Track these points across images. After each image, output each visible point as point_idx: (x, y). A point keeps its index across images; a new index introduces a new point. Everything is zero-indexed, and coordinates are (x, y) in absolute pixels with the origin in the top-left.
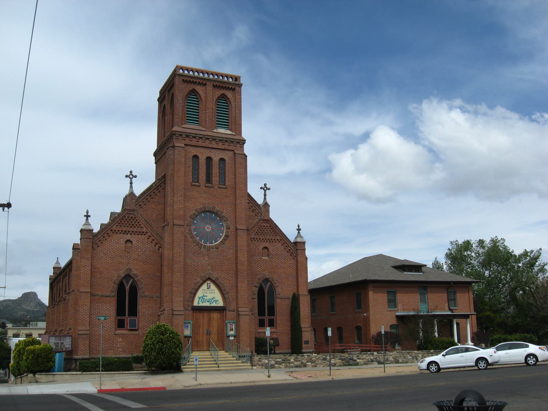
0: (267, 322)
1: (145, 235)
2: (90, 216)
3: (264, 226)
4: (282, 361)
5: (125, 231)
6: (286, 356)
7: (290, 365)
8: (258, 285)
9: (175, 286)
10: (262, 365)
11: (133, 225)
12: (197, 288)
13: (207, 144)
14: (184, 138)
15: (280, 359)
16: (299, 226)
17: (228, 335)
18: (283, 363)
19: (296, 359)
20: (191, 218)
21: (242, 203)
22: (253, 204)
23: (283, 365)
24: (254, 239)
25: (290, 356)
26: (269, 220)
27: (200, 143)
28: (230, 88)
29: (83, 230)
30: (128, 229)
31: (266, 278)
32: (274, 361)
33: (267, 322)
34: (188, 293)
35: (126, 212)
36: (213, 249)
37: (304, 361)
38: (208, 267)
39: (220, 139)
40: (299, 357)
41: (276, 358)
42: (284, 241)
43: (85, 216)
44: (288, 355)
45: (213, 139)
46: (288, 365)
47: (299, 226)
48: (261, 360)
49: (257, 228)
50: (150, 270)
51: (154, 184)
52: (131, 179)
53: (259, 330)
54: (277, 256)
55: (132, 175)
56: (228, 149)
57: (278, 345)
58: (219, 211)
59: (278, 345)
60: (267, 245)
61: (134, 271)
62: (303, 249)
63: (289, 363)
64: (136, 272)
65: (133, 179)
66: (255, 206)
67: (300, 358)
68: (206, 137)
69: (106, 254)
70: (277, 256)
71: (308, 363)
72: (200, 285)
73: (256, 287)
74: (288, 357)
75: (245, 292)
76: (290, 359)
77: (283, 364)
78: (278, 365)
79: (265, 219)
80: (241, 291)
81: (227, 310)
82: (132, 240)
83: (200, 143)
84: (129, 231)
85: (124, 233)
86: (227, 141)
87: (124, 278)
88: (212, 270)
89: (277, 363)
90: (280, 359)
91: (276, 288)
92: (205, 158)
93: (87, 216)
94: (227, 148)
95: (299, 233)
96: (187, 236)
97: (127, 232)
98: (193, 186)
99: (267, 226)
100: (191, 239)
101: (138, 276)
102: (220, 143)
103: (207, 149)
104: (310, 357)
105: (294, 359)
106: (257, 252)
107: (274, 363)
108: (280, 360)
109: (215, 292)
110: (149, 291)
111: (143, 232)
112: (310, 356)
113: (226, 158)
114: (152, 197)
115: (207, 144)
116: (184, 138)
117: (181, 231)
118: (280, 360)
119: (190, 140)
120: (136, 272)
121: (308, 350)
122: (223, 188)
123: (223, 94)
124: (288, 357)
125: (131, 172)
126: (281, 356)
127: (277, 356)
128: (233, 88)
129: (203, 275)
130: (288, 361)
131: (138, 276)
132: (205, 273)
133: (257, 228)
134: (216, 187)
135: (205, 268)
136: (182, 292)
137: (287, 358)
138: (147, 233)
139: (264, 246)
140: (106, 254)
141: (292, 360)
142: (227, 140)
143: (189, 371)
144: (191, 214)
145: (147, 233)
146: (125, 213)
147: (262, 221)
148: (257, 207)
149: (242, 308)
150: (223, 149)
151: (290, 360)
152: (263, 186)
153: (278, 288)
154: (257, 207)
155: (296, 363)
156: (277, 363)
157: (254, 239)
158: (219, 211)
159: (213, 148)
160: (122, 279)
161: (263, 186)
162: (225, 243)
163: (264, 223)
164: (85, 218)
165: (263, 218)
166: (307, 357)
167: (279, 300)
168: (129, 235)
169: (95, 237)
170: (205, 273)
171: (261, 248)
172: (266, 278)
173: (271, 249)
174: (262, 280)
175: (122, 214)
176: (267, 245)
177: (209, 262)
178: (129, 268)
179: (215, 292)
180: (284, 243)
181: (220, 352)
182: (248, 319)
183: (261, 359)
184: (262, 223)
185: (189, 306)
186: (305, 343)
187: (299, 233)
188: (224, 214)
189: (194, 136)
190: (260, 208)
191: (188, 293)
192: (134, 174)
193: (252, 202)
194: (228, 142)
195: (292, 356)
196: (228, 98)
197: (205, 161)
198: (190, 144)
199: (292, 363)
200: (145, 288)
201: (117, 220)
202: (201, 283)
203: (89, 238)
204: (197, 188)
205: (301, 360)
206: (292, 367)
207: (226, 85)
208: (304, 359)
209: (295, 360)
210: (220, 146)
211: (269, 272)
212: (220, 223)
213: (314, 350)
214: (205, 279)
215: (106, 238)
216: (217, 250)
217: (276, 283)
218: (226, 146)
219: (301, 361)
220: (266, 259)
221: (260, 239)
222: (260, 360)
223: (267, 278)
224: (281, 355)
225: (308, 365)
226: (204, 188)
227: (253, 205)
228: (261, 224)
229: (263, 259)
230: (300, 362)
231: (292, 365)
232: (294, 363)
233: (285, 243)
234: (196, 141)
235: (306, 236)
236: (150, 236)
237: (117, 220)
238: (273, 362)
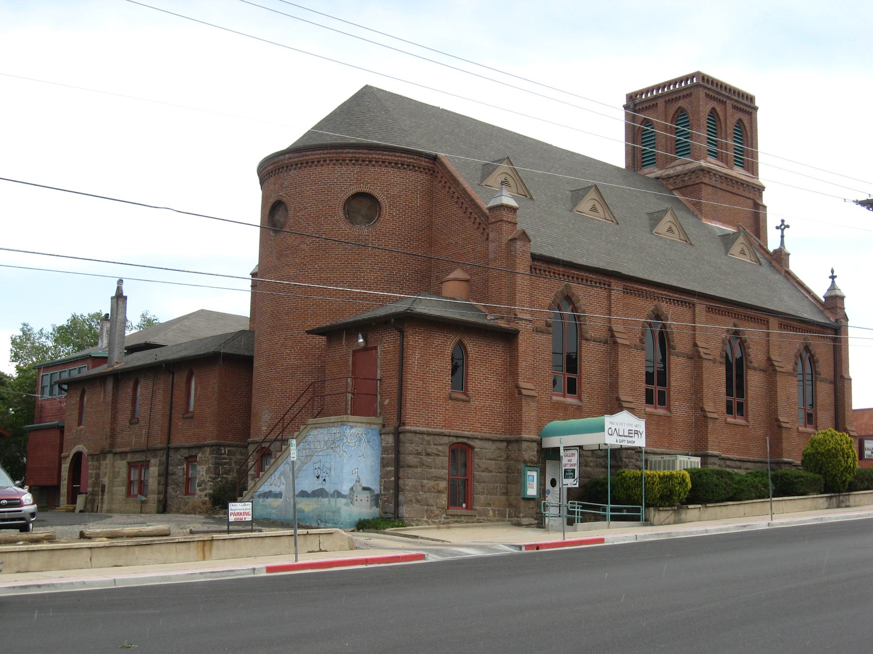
0: (656, 396)
2: (836, 277)
16: (832, 271)
27: (740, 192)
29: (503, 206)
33: (656, 396)
43: (830, 277)
47: (832, 271)
52: (783, 230)
55: (784, 228)
62: (833, 308)
65: (785, 231)
85: (341, 164)
93: (833, 277)
95: (833, 282)
109: (634, 430)
110: (491, 384)
125: (788, 226)
152: (786, 223)
161: (786, 223)
164: (831, 280)
179: (634, 430)
187: (833, 282)
192: (779, 224)
235: (843, 287)
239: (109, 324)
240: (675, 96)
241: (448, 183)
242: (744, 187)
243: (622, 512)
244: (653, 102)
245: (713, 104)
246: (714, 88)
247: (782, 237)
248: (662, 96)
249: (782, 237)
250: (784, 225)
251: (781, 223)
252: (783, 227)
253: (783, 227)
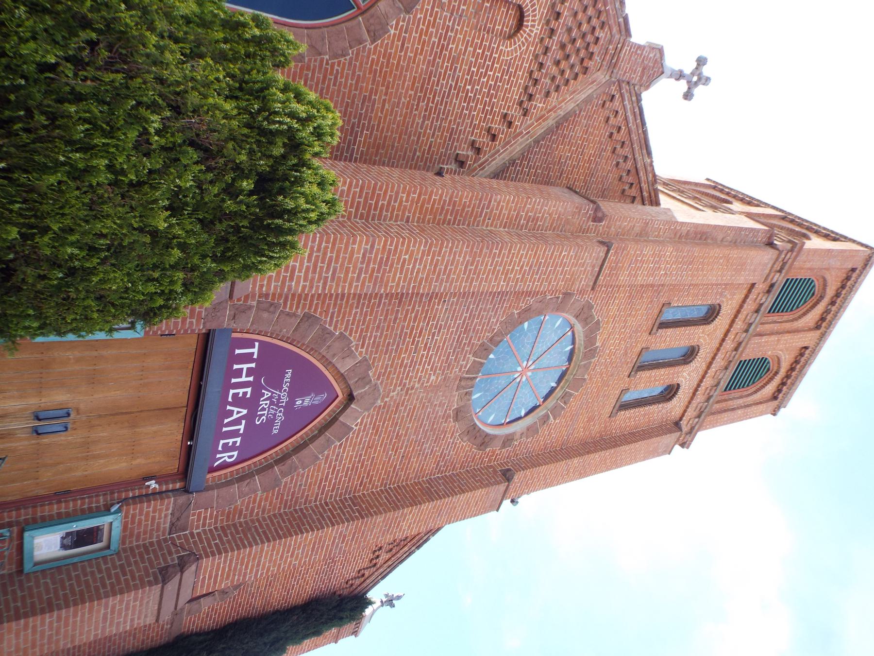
1: (521, 103)
9: (372, 246)
11: (567, 57)
30: (561, 35)
50: (387, 106)
51: (649, 161)
53: (56, 518)
55: (696, 84)
61: (397, 24)
64: (392, 32)
81: (182, 499)
82: (522, 36)
101: (373, 41)
111: (531, 97)
114: (483, 140)
120: (392, 32)
131: (373, 41)
136: (338, 285)
138: (525, 113)
145: (525, 113)
175: (616, 16)
200: (308, 69)
213: (80, 34)
216: (449, 416)
236: (510, 124)
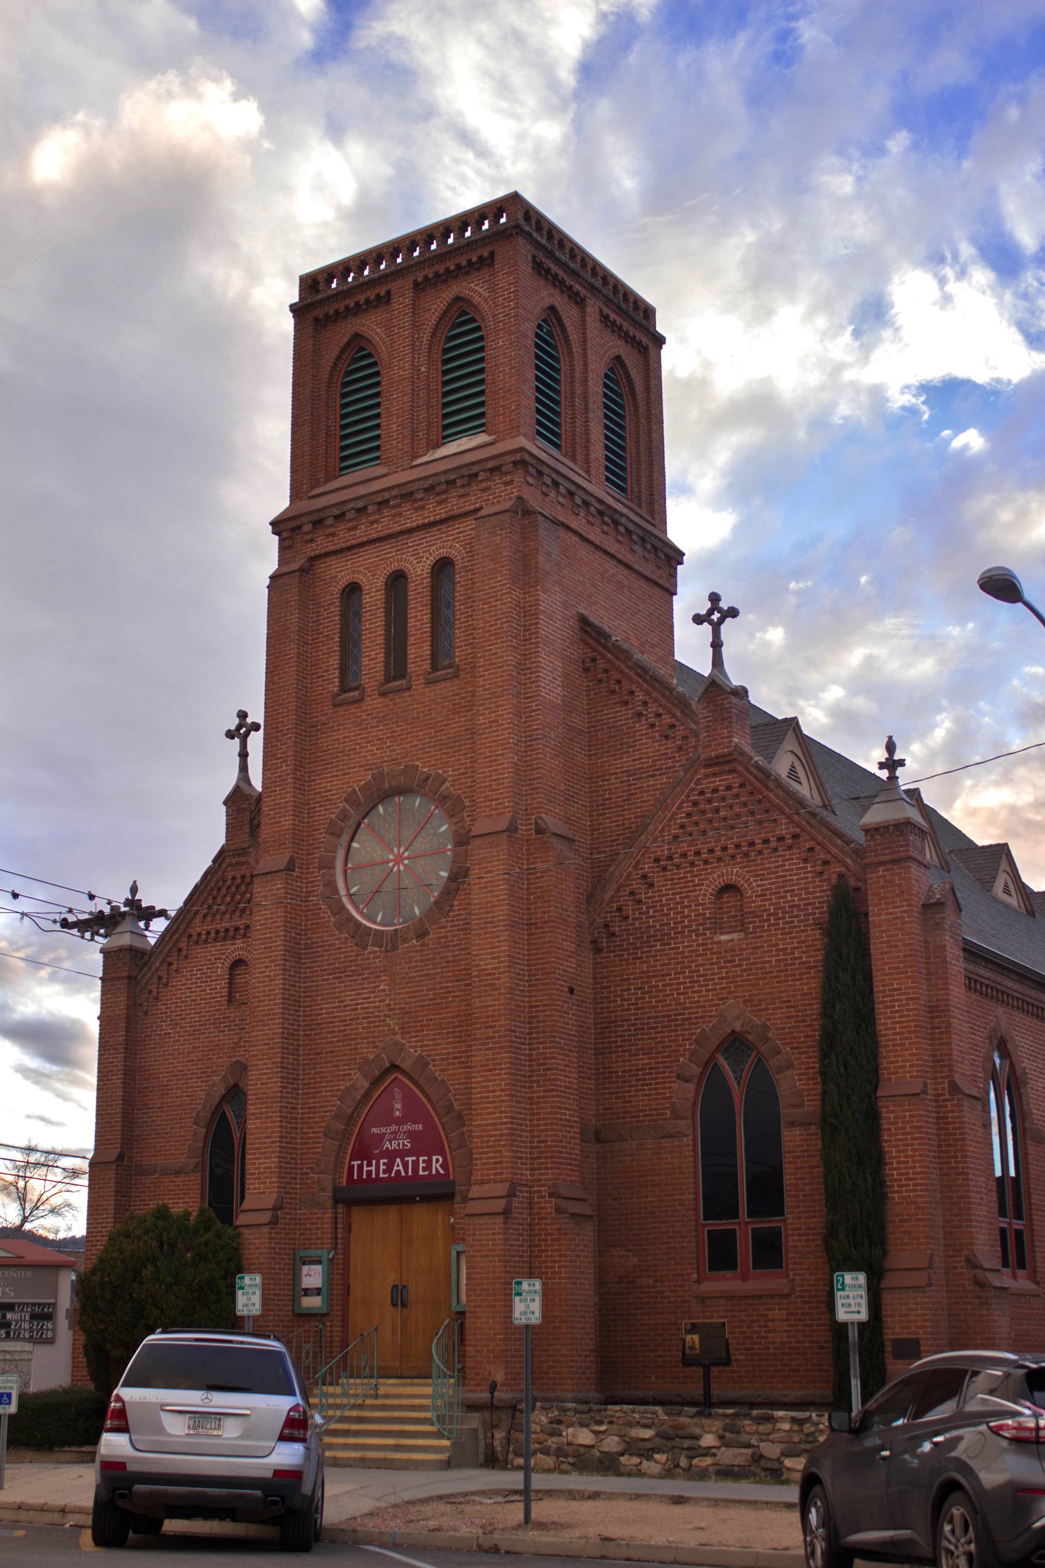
0: (744, 1248)
3: (715, 790)
4: (658, 1440)
5: (227, 930)
6: (679, 1414)
7: (695, 1462)
8: (696, 1070)
10: (559, 1452)
12: (350, 1111)
13: (386, 524)
14: (309, 537)
15: (647, 1430)
17: (299, 1311)
18: (659, 1451)
19: (728, 1435)
20: (331, 834)
21: (497, 721)
22: (661, 705)
23: (657, 1462)
24: (670, 858)
25: (700, 1414)
26: (730, 754)
28: (476, 263)
31: (733, 1031)
32: (616, 1438)
33: (744, 1248)
34: (319, 1137)
35: (227, 860)
36: (405, 940)
37: (771, 1450)
38: (388, 1021)
39: (425, 486)
40: (747, 1422)
41: (630, 1424)
42: (813, 839)
44: (693, 1410)
45: (402, 496)
46: (683, 1462)
48: (562, 1427)
49: (680, 807)
54: (783, 918)
55: (721, 621)
56: (461, 511)
57: (727, 1362)
58: (427, 779)
59: (727, 1362)
60: (733, 873)
63: (691, 1453)
66: (670, 712)
67: (748, 1429)
68: (379, 500)
69: (177, 1024)
70: (783, 918)
71: (788, 1463)
72: (359, 1097)
73: (688, 1080)
74: (686, 1419)
75: (500, 1112)
76: (697, 1431)
77: (657, 1456)
78: (635, 1460)
79: (713, 754)
80: (485, 1108)
83: (364, 531)
84: (237, 929)
86: (454, 481)
87: (223, 1099)
88: (404, 1028)
89: (632, 1447)
90: (646, 1426)
91: (781, 1075)
92: (380, 582)
94: (456, 512)
96: (320, 909)
97: (232, 933)
98: (340, 705)
99: (729, 788)
100: (332, 919)
102: (406, 509)
103: (385, 545)
104: (808, 1428)
105: (721, 1432)
106: (689, 916)
107: (620, 1449)
108: (648, 1433)
112: (808, 1420)
113: (456, 550)
115: (386, 524)
116: (309, 537)
117: (274, 895)
118: (648, 1433)
119: (328, 536)
121: (733, 1394)
122: (445, 680)
123: (458, 299)
124: (687, 1420)
126: (655, 1413)
127: (636, 1412)
128: (486, 254)
129: (371, 1057)
130: (686, 1443)
132: (377, 1047)
133: (680, 807)
134: (418, 684)
135: (379, 1026)
137: (683, 1427)
139: (721, 882)
140: (177, 1024)
141: (708, 1440)
142: (452, 477)
143: (424, 1462)
144: (332, 820)
146: (224, 866)
147: (706, 766)
148: (678, 714)
149: (488, 1182)
150: (442, 521)
151: (698, 1438)
152: (724, 605)
153: (789, 1073)
154: (678, 714)
155: (728, 1456)
156: (632, 1447)
157: (670, 858)
158: (427, 779)
159: (411, 531)
160: (219, 1105)
161: (724, 605)
162: (452, 906)
163: (715, 775)
165: (703, 757)
166: (786, 1426)
167: (797, 1131)
168: (239, 944)
169: (145, 969)
170: (377, 1047)
171: (706, 892)
172: (733, 1031)
173: (752, 887)
174: (715, 1042)
176: (733, 873)
177: (391, 1000)
178: (238, 1062)
180: (811, 850)
181: (384, 1384)
182: (500, 1234)
183: (560, 1422)
184: (706, 776)
185: (323, 1189)
186: (898, 1355)
188: (447, 784)
189: (338, 512)
190: (692, 711)
191: (319, 1137)
192: (233, 723)
193: (655, 694)
194: (459, 482)
195: (709, 1416)
196: (448, 308)
197: (380, 596)
198: (333, 548)
199: (707, 1452)
201: (202, 898)
202: (363, 1091)
203: (119, 978)
204: (352, 709)
205: (753, 1442)
206: (702, 1475)
207: (458, 260)
208: (771, 1437)
209: (721, 1437)
210: (434, 511)
211: (745, 1002)
212: (440, 827)
214: (377, 1073)
215: (174, 967)
216: (423, 945)
217: (779, 1052)
218: (455, 504)
219: (753, 1446)
220: (732, 940)
221: (698, 853)
222: (554, 1429)
223: (738, 1029)
224: (657, 1408)
225: (788, 1469)
226: (379, 702)
227: (665, 708)
228: (697, 783)
229: (719, 942)
230: (749, 1451)
231: (703, 1464)
232: (714, 1455)
233: (817, 848)
234: (350, 529)
237: (202, 898)
238: (612, 1444)
239: (517, 1314)
240: (433, 270)
241: (604, 685)
242: (617, 530)
243: (920, 1359)
244: (377, 290)
245: (549, 296)
246: (564, 258)
247: (717, 645)
248: (398, 273)
249: (717, 645)
250: (720, 610)
251: (237, 721)
252: (716, 616)
253: (716, 616)
